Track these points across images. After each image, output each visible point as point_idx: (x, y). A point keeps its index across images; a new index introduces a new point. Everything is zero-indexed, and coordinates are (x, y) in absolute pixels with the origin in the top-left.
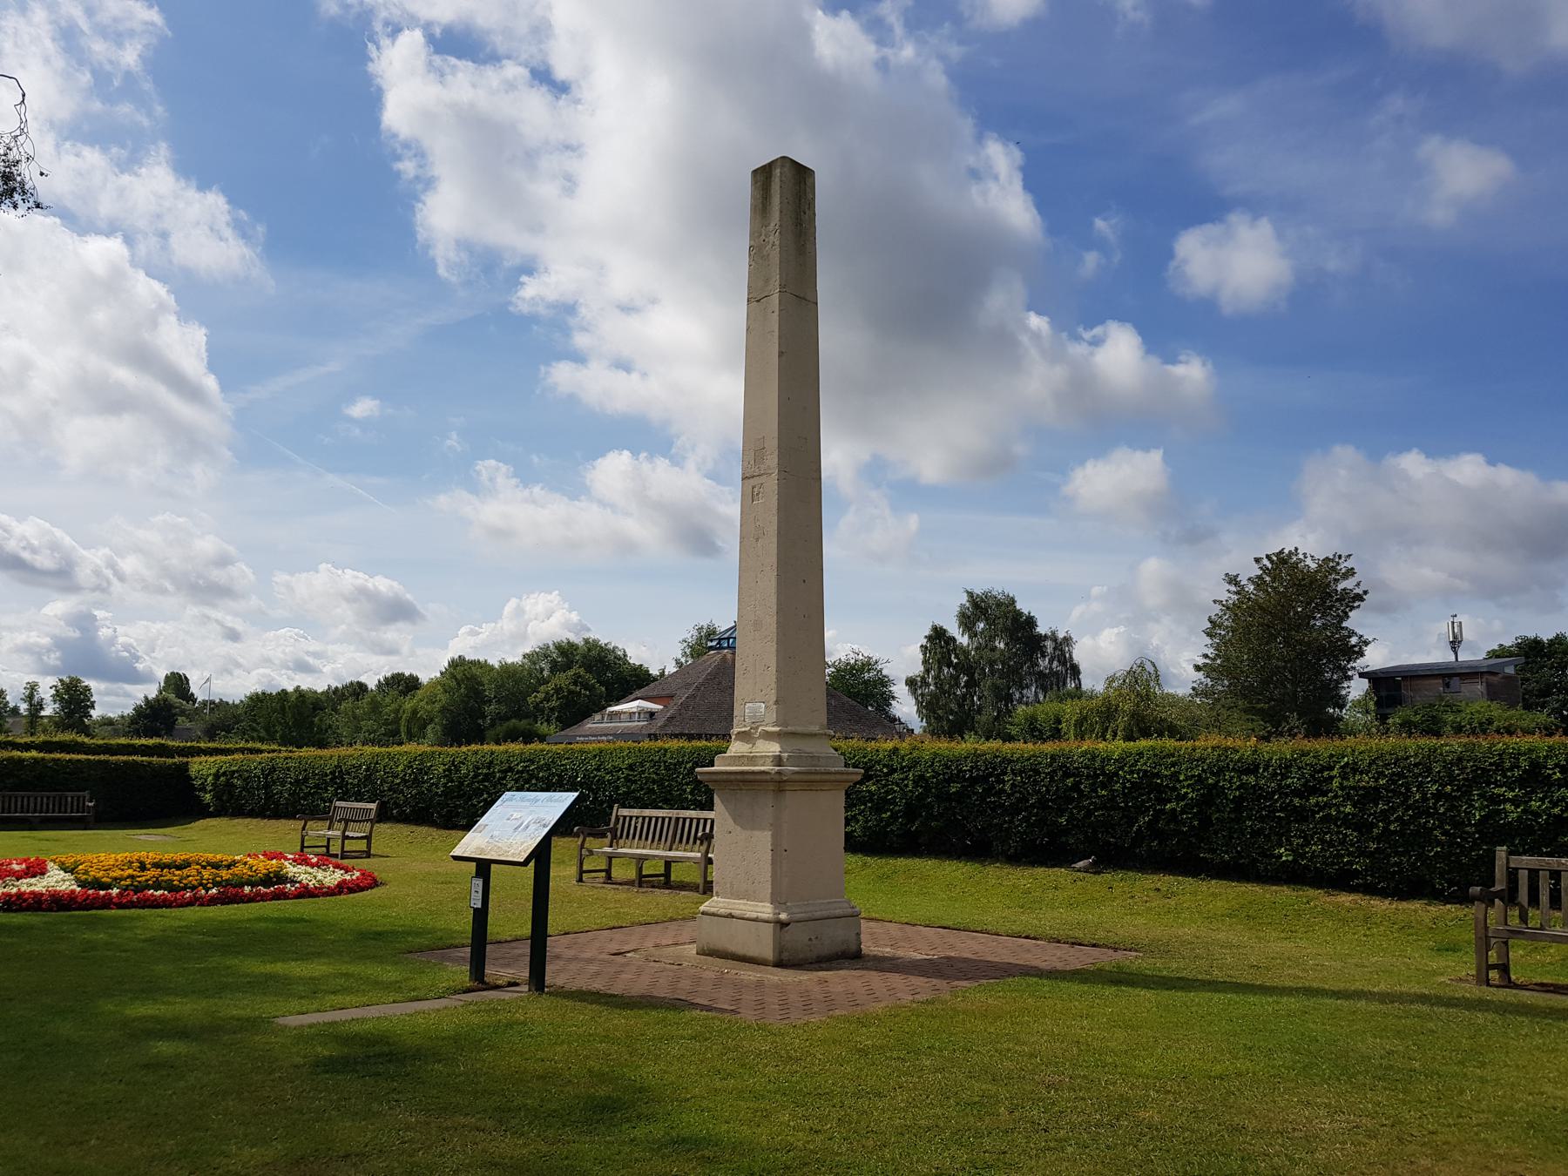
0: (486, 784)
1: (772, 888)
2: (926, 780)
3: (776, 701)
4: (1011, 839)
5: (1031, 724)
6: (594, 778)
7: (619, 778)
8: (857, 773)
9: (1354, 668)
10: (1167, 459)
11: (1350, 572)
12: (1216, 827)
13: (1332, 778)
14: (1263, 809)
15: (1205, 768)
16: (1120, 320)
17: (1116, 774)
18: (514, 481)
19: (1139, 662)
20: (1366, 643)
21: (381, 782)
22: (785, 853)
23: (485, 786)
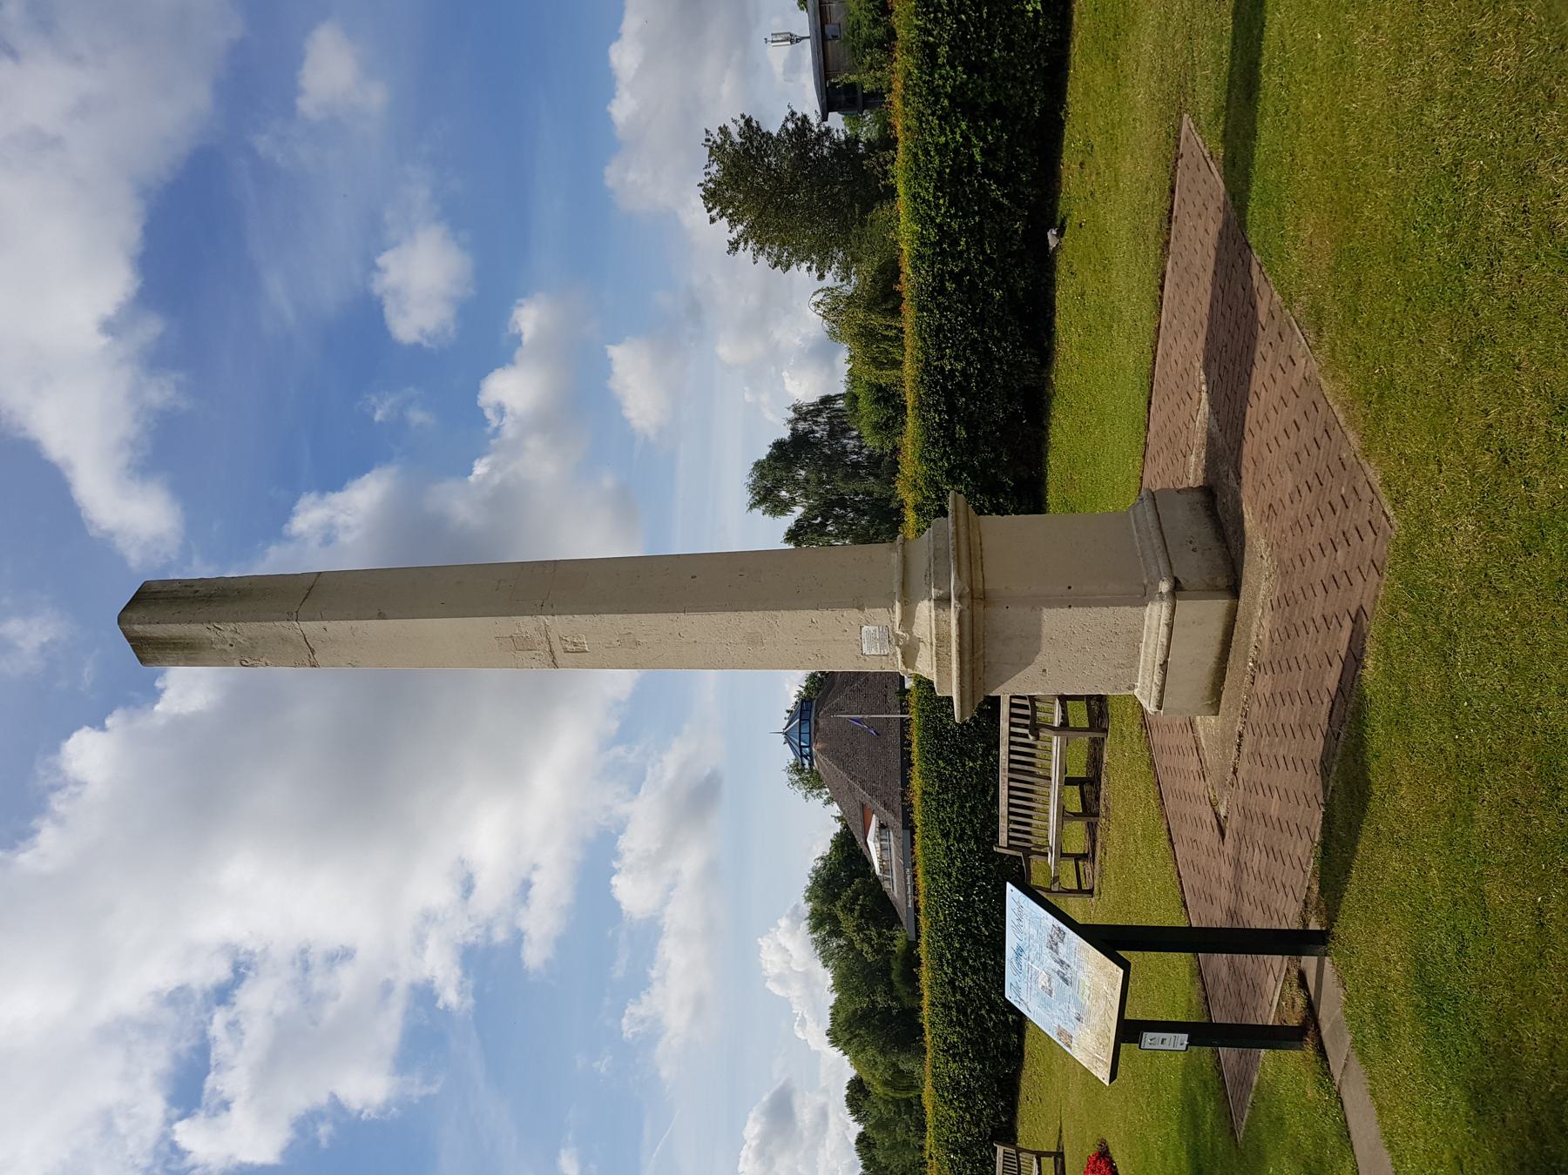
0: (969, 1011)
1: (1125, 605)
2: (954, 467)
3: (858, 608)
4: (1021, 361)
5: (881, 428)
6: (959, 880)
7: (959, 850)
8: (955, 499)
9: (818, 126)
10: (616, 341)
11: (724, 130)
12: (1001, 98)
14: (978, 36)
15: (930, 112)
16: (478, 393)
17: (940, 226)
18: (644, 997)
19: (813, 307)
20: (793, 114)
21: (969, 1136)
22: (1072, 587)
23: (971, 1013)
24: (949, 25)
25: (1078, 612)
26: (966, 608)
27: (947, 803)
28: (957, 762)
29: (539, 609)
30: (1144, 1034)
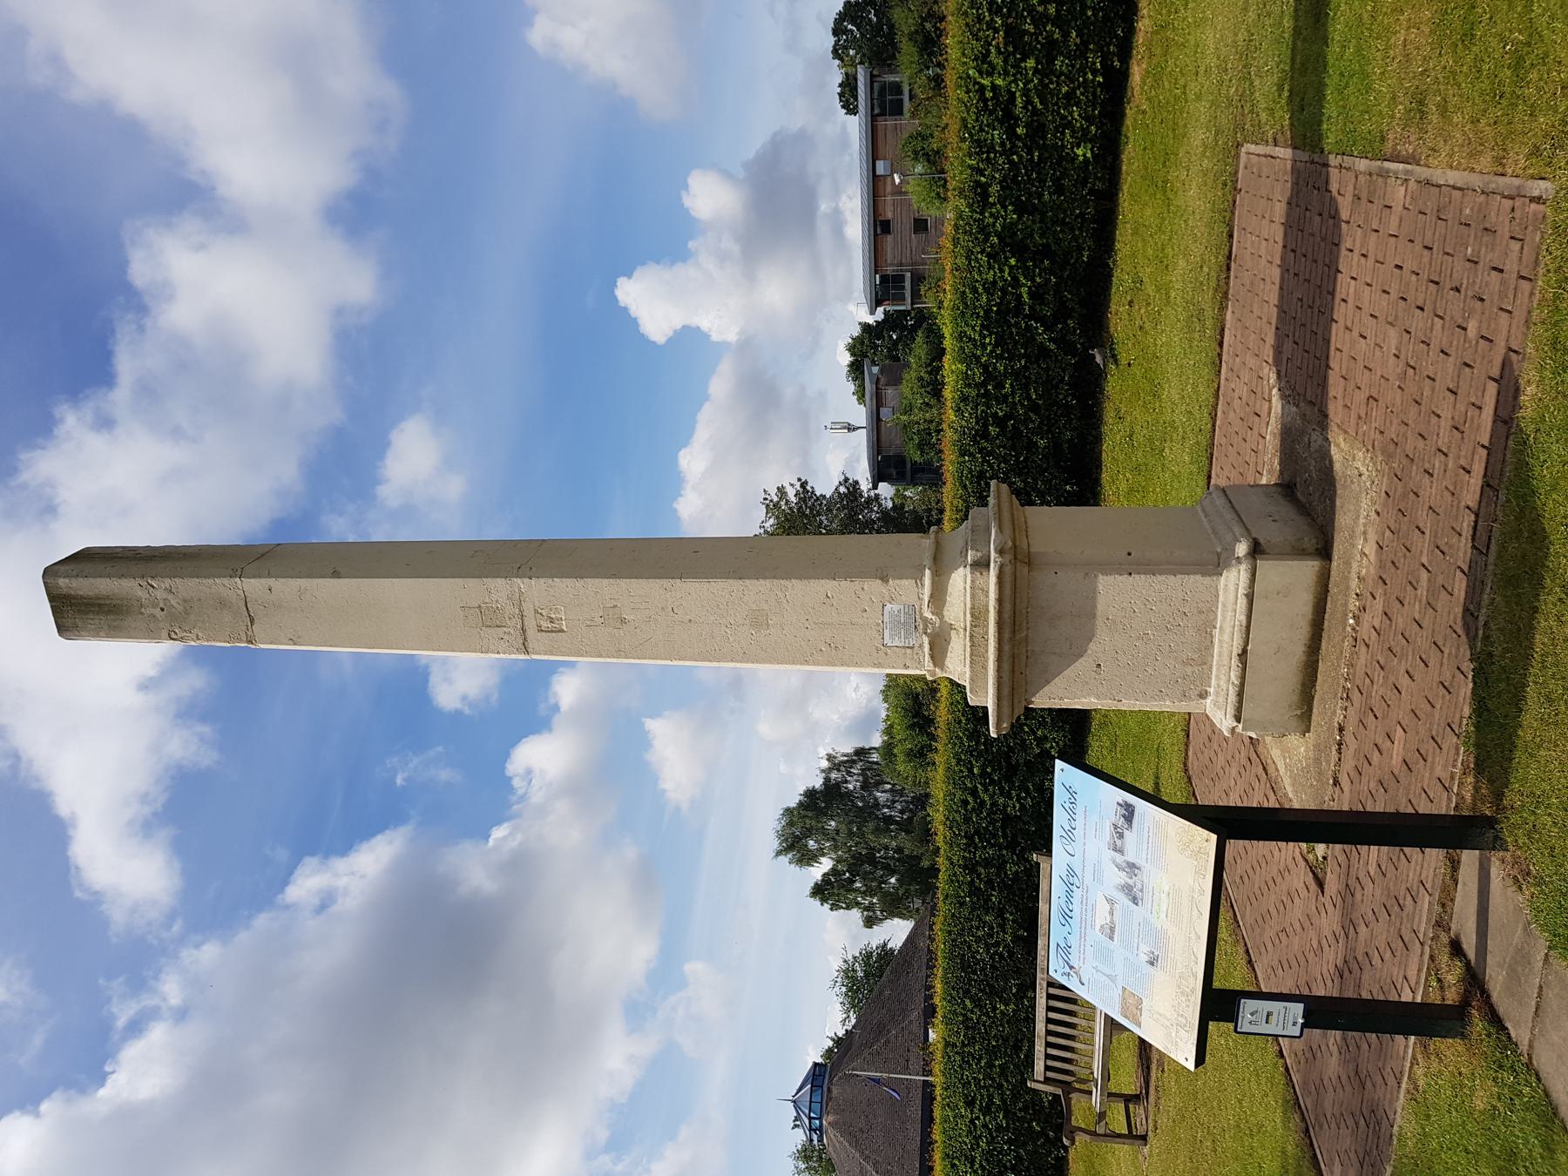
7: (985, 1126)
8: (998, 491)
10: (656, 714)
13: (994, 87)
17: (985, 367)
20: (846, 480)
24: (1000, 165)
25: (1140, 580)
26: (1008, 562)
27: (974, 1058)
28: (986, 1004)
29: (515, 571)
30: (1242, 1001)
